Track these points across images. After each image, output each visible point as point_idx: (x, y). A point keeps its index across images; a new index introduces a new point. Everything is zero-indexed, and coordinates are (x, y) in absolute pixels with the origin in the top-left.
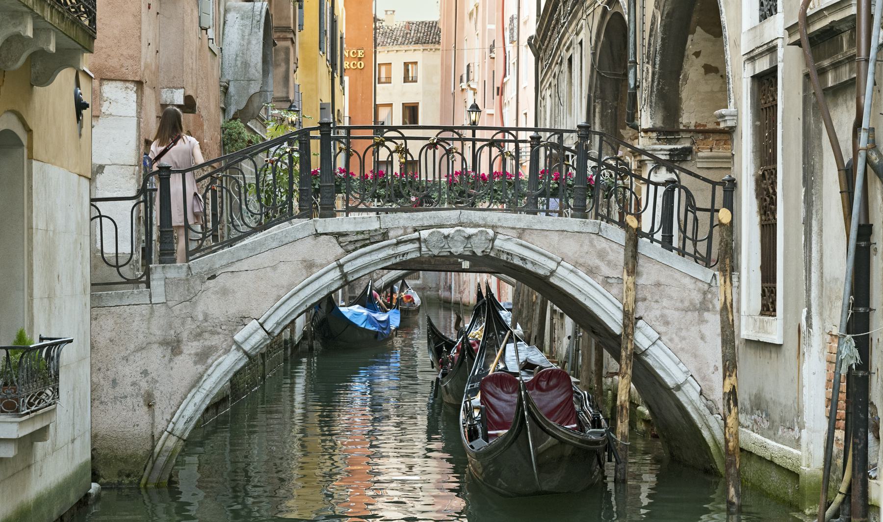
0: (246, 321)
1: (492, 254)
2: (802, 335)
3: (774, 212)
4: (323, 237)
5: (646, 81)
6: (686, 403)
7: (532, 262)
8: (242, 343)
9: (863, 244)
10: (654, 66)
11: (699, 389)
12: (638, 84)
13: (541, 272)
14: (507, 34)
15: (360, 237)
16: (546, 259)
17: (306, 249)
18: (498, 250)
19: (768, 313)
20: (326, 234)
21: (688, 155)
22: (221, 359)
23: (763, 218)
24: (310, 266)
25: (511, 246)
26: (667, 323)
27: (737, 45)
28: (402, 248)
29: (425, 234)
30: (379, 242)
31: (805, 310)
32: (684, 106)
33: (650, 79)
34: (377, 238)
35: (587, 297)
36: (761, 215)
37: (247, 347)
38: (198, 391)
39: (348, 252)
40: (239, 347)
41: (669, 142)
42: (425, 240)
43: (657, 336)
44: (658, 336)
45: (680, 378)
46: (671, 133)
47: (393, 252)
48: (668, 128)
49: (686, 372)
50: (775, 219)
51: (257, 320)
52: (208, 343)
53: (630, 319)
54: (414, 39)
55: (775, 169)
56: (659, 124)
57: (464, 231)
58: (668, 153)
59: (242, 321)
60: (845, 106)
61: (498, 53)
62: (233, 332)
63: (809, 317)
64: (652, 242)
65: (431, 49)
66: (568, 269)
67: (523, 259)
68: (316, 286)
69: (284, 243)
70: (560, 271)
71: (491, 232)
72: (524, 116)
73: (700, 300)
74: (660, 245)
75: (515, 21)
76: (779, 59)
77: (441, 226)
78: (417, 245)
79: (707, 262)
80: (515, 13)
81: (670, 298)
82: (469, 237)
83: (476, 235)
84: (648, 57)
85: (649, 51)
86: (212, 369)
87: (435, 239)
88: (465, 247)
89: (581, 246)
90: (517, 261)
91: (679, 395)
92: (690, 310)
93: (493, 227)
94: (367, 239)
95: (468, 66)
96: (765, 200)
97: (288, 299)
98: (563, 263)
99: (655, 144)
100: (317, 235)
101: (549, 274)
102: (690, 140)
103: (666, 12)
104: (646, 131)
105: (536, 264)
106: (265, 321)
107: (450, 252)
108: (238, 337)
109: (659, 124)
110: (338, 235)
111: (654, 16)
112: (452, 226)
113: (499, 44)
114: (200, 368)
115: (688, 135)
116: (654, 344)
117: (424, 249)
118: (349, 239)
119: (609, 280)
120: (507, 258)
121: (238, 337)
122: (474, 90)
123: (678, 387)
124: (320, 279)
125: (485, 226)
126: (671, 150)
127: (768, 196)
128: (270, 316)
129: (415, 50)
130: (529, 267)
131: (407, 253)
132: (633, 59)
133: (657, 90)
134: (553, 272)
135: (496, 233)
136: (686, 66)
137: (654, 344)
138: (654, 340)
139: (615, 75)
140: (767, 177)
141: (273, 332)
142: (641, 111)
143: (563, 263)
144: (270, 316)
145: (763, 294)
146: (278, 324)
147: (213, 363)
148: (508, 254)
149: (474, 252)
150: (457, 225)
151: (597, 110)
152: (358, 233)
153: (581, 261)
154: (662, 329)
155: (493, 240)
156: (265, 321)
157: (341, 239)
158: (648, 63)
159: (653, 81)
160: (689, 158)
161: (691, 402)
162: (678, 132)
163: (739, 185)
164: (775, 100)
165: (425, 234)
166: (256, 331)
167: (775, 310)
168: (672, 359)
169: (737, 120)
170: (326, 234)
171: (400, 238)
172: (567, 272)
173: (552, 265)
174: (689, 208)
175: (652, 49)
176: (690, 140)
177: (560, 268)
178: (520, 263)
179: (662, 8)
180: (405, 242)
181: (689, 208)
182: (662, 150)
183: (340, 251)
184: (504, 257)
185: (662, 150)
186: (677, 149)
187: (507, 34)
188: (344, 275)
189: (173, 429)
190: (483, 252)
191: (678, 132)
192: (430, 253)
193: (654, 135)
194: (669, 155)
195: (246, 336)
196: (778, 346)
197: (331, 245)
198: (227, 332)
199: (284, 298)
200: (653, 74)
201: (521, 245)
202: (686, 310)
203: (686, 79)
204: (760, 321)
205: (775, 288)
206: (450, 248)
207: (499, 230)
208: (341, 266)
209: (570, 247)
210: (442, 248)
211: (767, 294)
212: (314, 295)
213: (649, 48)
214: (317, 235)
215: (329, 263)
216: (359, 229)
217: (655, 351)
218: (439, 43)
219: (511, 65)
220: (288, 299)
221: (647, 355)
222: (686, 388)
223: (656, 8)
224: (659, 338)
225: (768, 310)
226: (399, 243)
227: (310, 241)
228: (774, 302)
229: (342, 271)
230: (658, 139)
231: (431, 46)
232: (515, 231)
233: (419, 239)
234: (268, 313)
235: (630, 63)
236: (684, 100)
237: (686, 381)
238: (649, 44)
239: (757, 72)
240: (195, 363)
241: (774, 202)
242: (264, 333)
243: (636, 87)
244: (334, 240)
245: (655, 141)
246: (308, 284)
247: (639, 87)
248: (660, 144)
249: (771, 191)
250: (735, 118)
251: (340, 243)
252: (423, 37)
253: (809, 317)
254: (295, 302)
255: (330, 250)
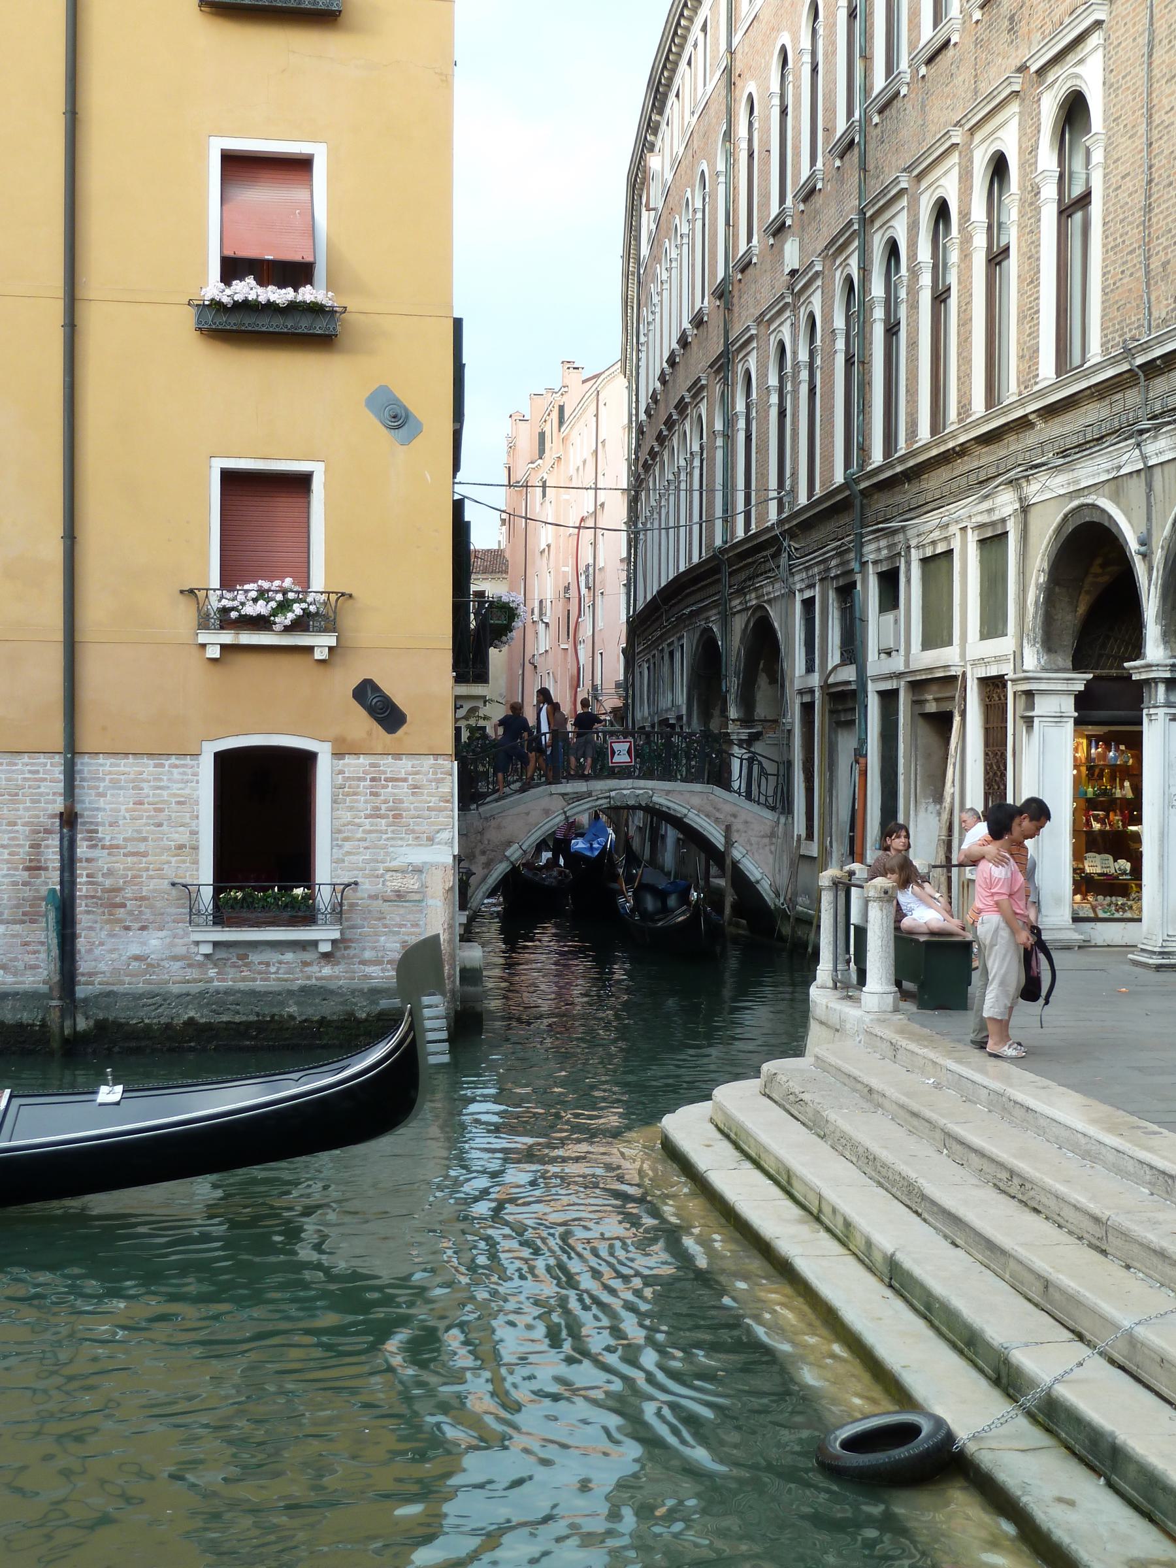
17: (545, 802)
25: (662, 801)
27: (792, 682)
29: (613, 794)
32: (758, 705)
37: (512, 859)
45: (759, 876)
53: (729, 843)
56: (742, 716)
59: (509, 844)
60: (577, 1277)
62: (505, 850)
63: (831, 842)
68: (551, 824)
75: (591, 569)
79: (773, 809)
80: (591, 561)
91: (758, 886)
94: (579, 797)
95: (541, 602)
100: (552, 794)
108: (507, 853)
110: (563, 795)
113: (574, 588)
114: (486, 871)
121: (507, 853)
122: (547, 624)
123: (758, 882)
162: (754, 721)
165: (613, 794)
173: (685, 811)
182: (744, 733)
185: (744, 733)
188: (567, 818)
191: (754, 721)
202: (763, 837)
203: (759, 687)
209: (696, 801)
214: (552, 794)
217: (744, 860)
218: (506, 572)
231: (498, 576)
243: (727, 691)
253: (831, 842)
255: (559, 803)
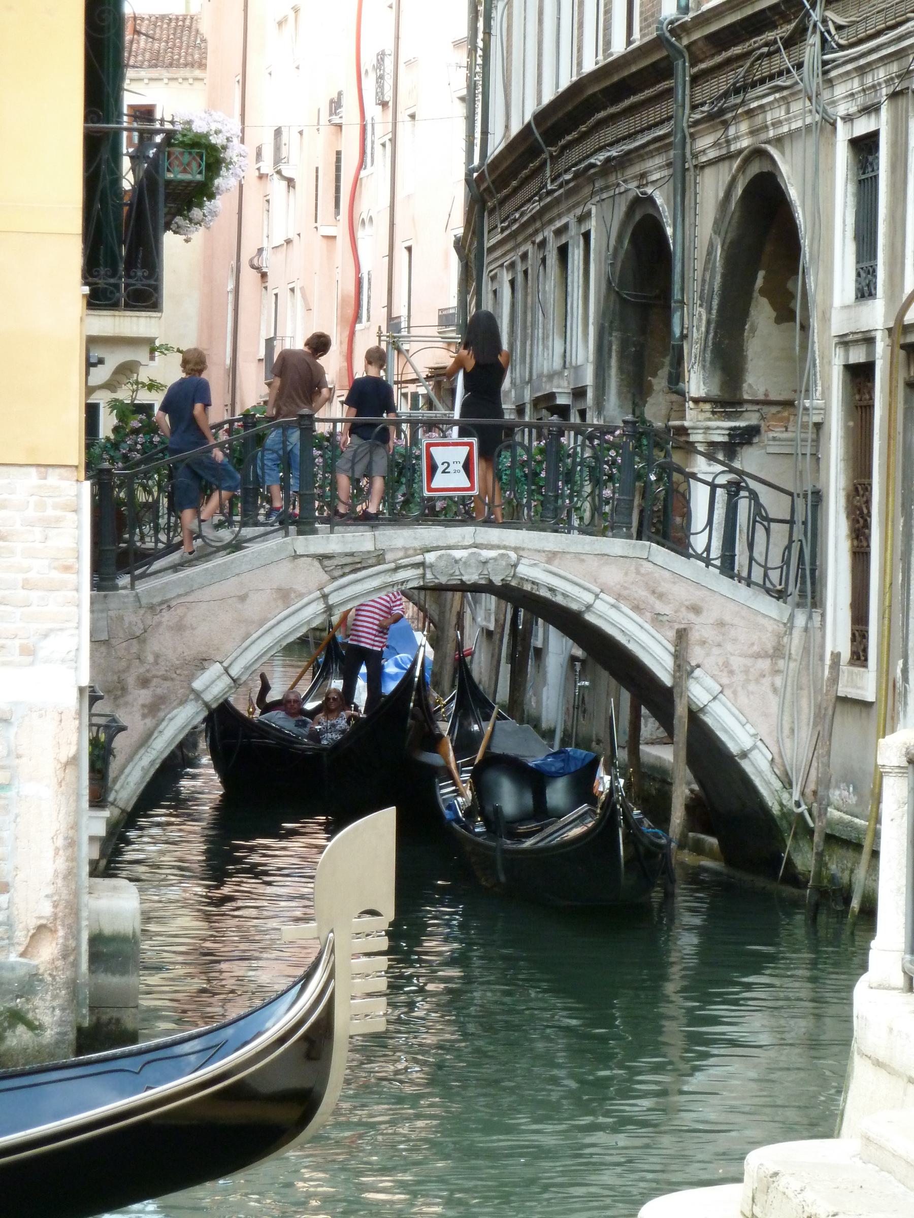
0: (206, 664)
1: (513, 583)
2: (897, 691)
3: (868, 538)
4: (303, 559)
5: (698, 330)
6: (754, 774)
7: (563, 594)
8: (204, 690)
9: (314, 1203)
10: (709, 312)
11: (770, 757)
12: (685, 332)
13: (574, 606)
14: (369, 85)
15: (349, 560)
16: (581, 590)
17: (282, 574)
18: (521, 578)
19: (858, 662)
20: (307, 556)
21: (755, 436)
22: (175, 712)
23: (855, 543)
24: (285, 595)
26: (731, 672)
28: (402, 575)
29: (430, 557)
30: (372, 566)
31: (900, 663)
33: (703, 329)
34: (370, 562)
35: (631, 638)
36: (852, 540)
37: (208, 697)
38: (146, 751)
39: (334, 579)
40: (198, 695)
41: (729, 416)
42: (431, 566)
43: (719, 689)
44: (720, 689)
46: (732, 404)
47: (390, 580)
48: (727, 397)
49: (755, 735)
50: (869, 546)
51: (221, 663)
52: (159, 691)
54: (147, 55)
55: (870, 485)
56: (715, 392)
57: (480, 555)
58: (727, 432)
59: (202, 663)
61: (350, 114)
62: (192, 677)
64: (707, 566)
65: (185, 79)
66: (608, 603)
67: (552, 590)
69: (255, 567)
70: (599, 606)
71: (513, 556)
72: (406, 253)
73: (774, 644)
74: (717, 571)
76: (877, 356)
77: (449, 548)
78: (420, 571)
79: (781, 595)
81: (735, 640)
82: (485, 563)
83: (495, 559)
84: (701, 298)
85: (702, 290)
86: (164, 724)
87: (443, 563)
88: (480, 574)
89: (626, 574)
90: (544, 593)
92: (761, 657)
93: (516, 549)
96: (858, 522)
97: (259, 638)
98: (602, 595)
99: (709, 419)
101: (584, 609)
102: (757, 415)
103: (728, 241)
104: (696, 401)
105: (568, 596)
106: (230, 665)
107: (461, 580)
108: (197, 685)
109: (715, 392)
110: (322, 558)
111: (711, 245)
112: (465, 548)
114: (149, 722)
115: (756, 408)
116: (715, 698)
117: (429, 576)
118: (335, 562)
119: (661, 618)
120: (532, 588)
121: (197, 685)
122: (290, 182)
123: (744, 755)
124: (300, 612)
125: (505, 548)
126: (731, 429)
127: (862, 517)
128: (236, 658)
129: (151, 79)
130: (559, 599)
131: (408, 581)
132: (679, 297)
133: (713, 344)
134: (589, 607)
135: (520, 557)
136: (753, 312)
137: (715, 698)
138: (715, 694)
139: (645, 297)
140: (861, 492)
141: (238, 679)
142: (689, 371)
143: (602, 595)
144: (236, 658)
145: (854, 639)
146: (246, 668)
147: (165, 716)
148: (533, 583)
149: (491, 581)
150: (470, 546)
151: (614, 347)
152: (347, 555)
153: (625, 593)
154: (725, 681)
155: (515, 566)
156: (230, 665)
157: (326, 562)
158: (701, 306)
159: (707, 332)
160: (756, 440)
161: (760, 773)
162: (741, 403)
163: (824, 499)
164: (872, 398)
165: (430, 557)
166: (219, 677)
167: (866, 660)
168: (737, 719)
169: (825, 414)
170: (307, 556)
171: (399, 562)
172: (609, 606)
173: (588, 598)
174: (758, 519)
175: (707, 287)
176: (757, 415)
177: (598, 601)
178: (548, 595)
179: (723, 233)
180: (405, 566)
181: (758, 519)
183: (326, 577)
184: (527, 587)
186: (738, 428)
187: (369, 85)
189: (115, 800)
190: (502, 580)
191: (741, 403)
192: (436, 581)
193: (708, 407)
194: (729, 435)
195: (208, 683)
196: (867, 705)
197: (313, 569)
198: (182, 678)
199: (255, 636)
200: (708, 322)
201: (551, 572)
202: (757, 656)
203: (753, 330)
204: (849, 672)
205: (867, 632)
206: (461, 574)
207: (521, 553)
208: (325, 597)
209: (612, 575)
210: (452, 575)
211: (858, 639)
212: (291, 633)
213: (703, 285)
214: (296, 556)
215: (310, 593)
216: (348, 550)
218: (202, 66)
219: (378, 148)
220: (259, 638)
221: (705, 714)
222: (755, 755)
223: (715, 232)
224: (721, 692)
225: (859, 659)
226: (396, 569)
227: (287, 566)
228: (865, 650)
229: (326, 602)
230: (713, 413)
232: (543, 554)
233: (422, 564)
234: (235, 655)
235: (675, 302)
236: (749, 358)
237: (754, 747)
238: (704, 281)
239: (854, 136)
240: (144, 716)
241: (867, 525)
242: (229, 681)
243: (684, 337)
244: (316, 563)
245: (709, 415)
246: (285, 619)
247: (686, 336)
248: (715, 420)
249: (865, 511)
250: (822, 412)
251: (324, 567)
252: (165, 50)
254: (267, 641)
255: (315, 575)
